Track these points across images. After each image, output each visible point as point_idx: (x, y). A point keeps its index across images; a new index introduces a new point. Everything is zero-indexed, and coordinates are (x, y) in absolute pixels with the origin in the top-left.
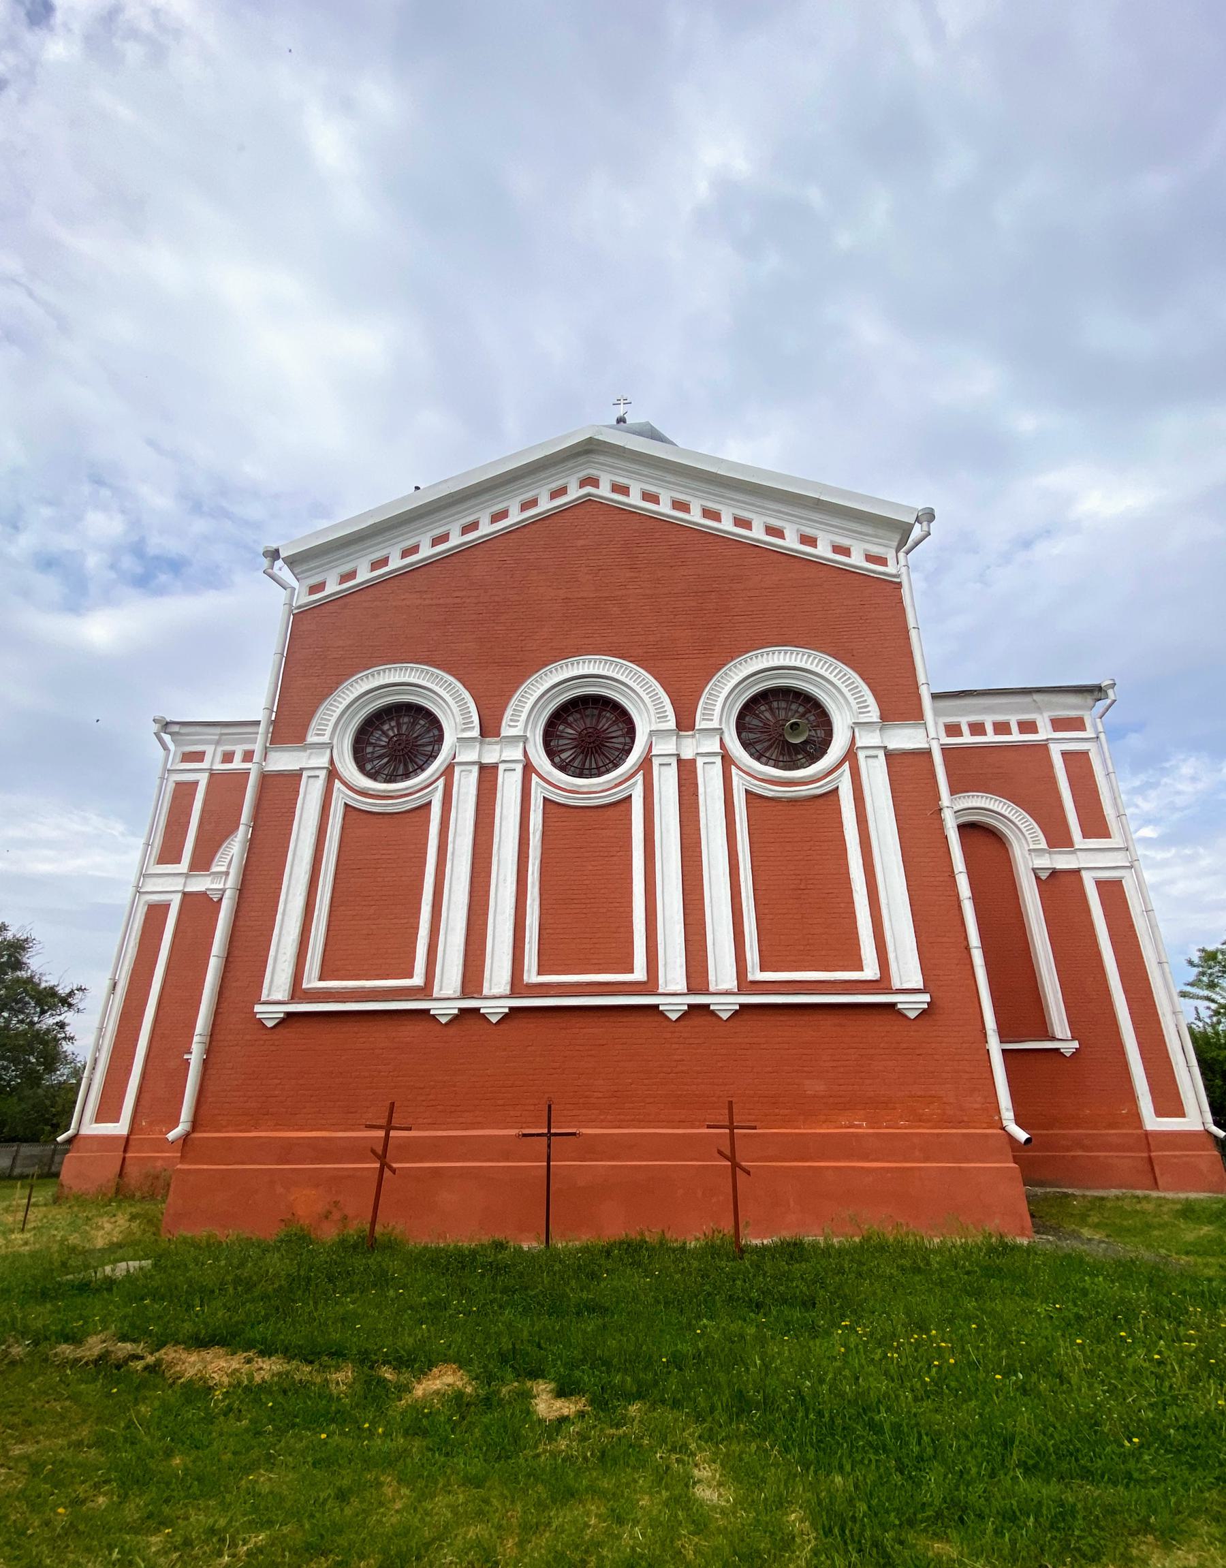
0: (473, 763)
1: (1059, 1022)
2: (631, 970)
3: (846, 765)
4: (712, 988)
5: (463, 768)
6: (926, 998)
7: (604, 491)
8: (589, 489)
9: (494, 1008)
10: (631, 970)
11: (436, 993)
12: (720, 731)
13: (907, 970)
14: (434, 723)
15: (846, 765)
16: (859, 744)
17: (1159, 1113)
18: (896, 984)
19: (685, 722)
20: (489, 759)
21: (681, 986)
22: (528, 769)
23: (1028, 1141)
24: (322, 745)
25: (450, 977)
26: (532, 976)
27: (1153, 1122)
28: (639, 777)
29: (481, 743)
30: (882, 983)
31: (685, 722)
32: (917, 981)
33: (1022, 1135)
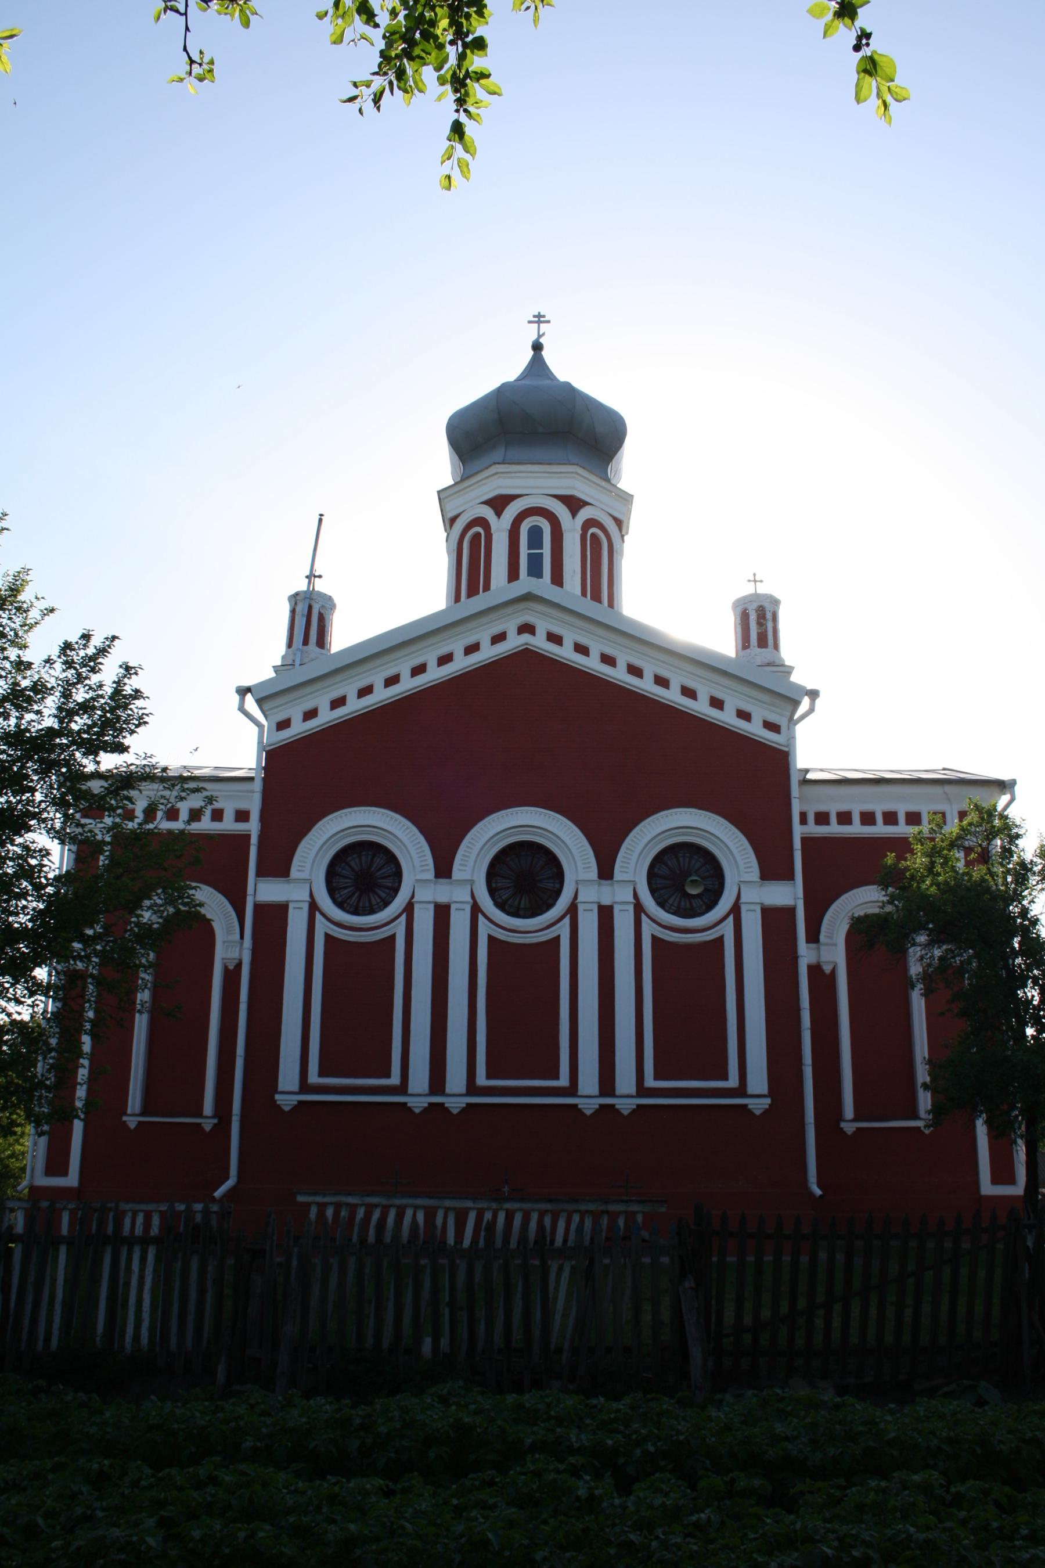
0: (429, 902)
1: (208, 1108)
2: (557, 1078)
3: (731, 918)
4: (618, 1092)
5: (459, 906)
6: (768, 1101)
7: (539, 642)
8: (526, 638)
9: (625, 1105)
10: (557, 1078)
11: (410, 1091)
12: (472, 882)
13: (758, 1081)
14: (392, 859)
15: (568, 917)
16: (743, 900)
17: (995, 1181)
18: (750, 1090)
19: (606, 872)
20: (443, 899)
21: (596, 1091)
22: (314, 907)
23: (821, 1196)
24: (305, 880)
25: (589, 1081)
26: (313, 1078)
27: (987, 1188)
28: (567, 920)
29: (599, 884)
30: (741, 1091)
31: (606, 872)
32: (764, 1089)
33: (818, 1192)
